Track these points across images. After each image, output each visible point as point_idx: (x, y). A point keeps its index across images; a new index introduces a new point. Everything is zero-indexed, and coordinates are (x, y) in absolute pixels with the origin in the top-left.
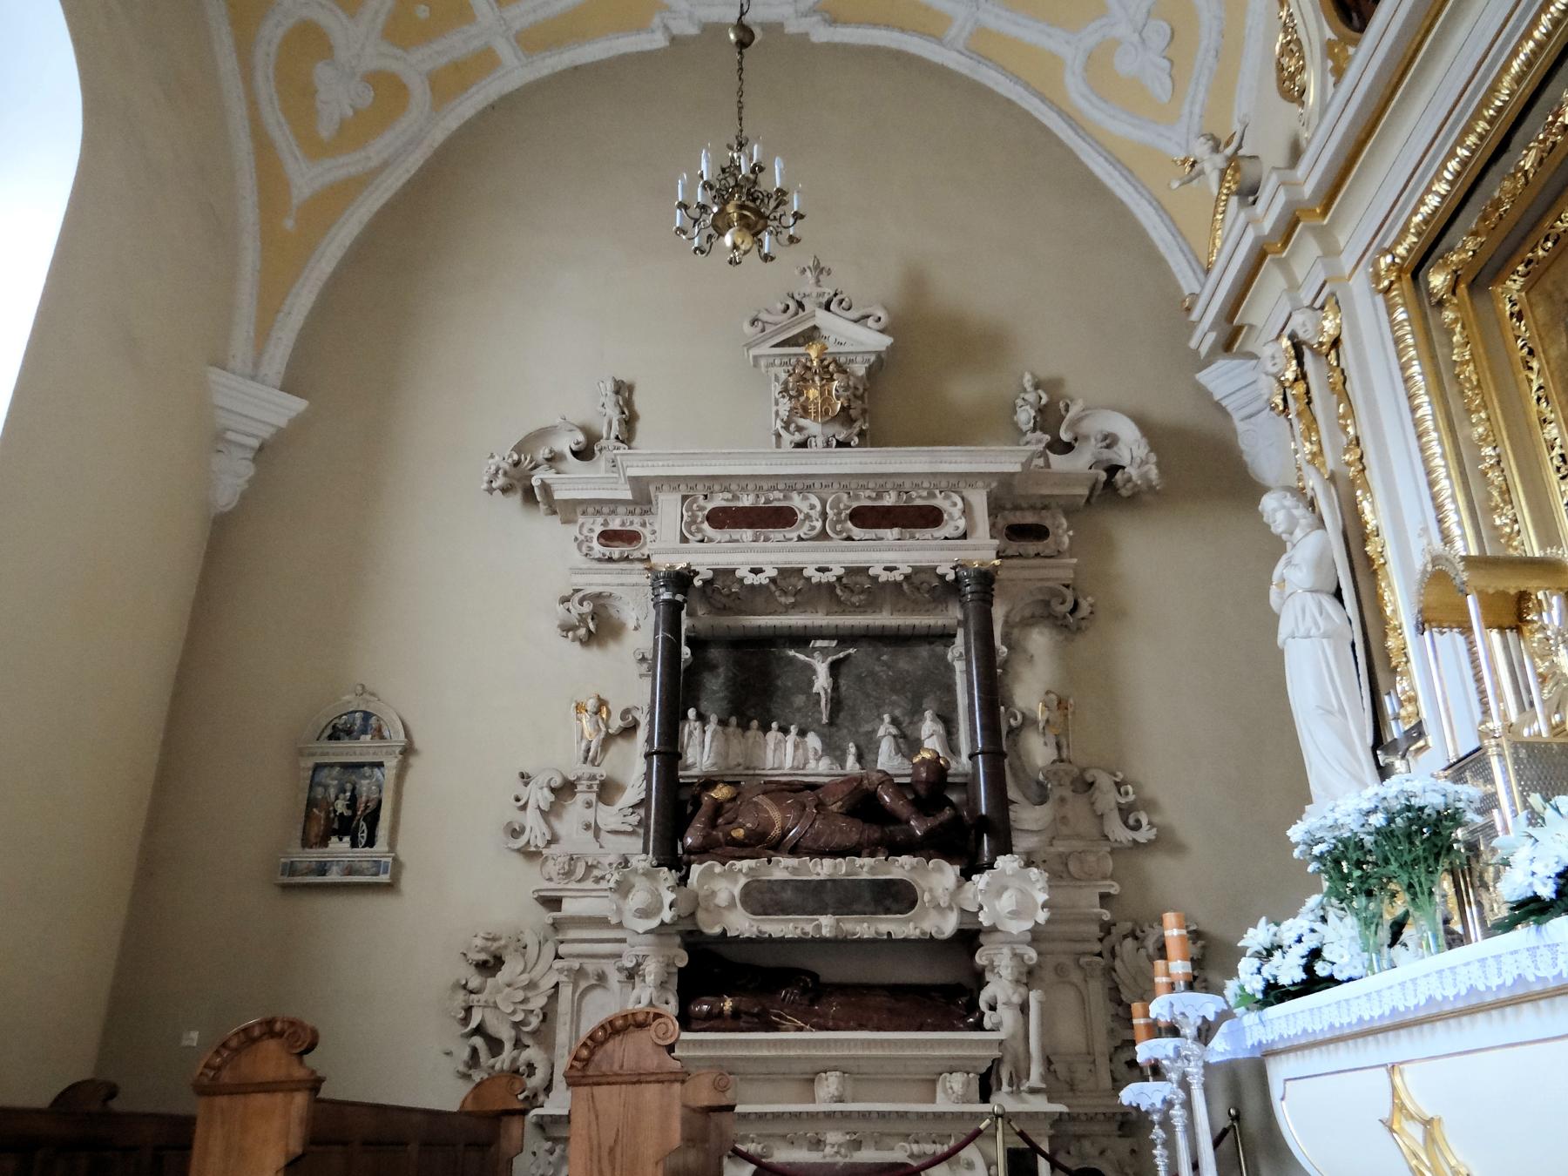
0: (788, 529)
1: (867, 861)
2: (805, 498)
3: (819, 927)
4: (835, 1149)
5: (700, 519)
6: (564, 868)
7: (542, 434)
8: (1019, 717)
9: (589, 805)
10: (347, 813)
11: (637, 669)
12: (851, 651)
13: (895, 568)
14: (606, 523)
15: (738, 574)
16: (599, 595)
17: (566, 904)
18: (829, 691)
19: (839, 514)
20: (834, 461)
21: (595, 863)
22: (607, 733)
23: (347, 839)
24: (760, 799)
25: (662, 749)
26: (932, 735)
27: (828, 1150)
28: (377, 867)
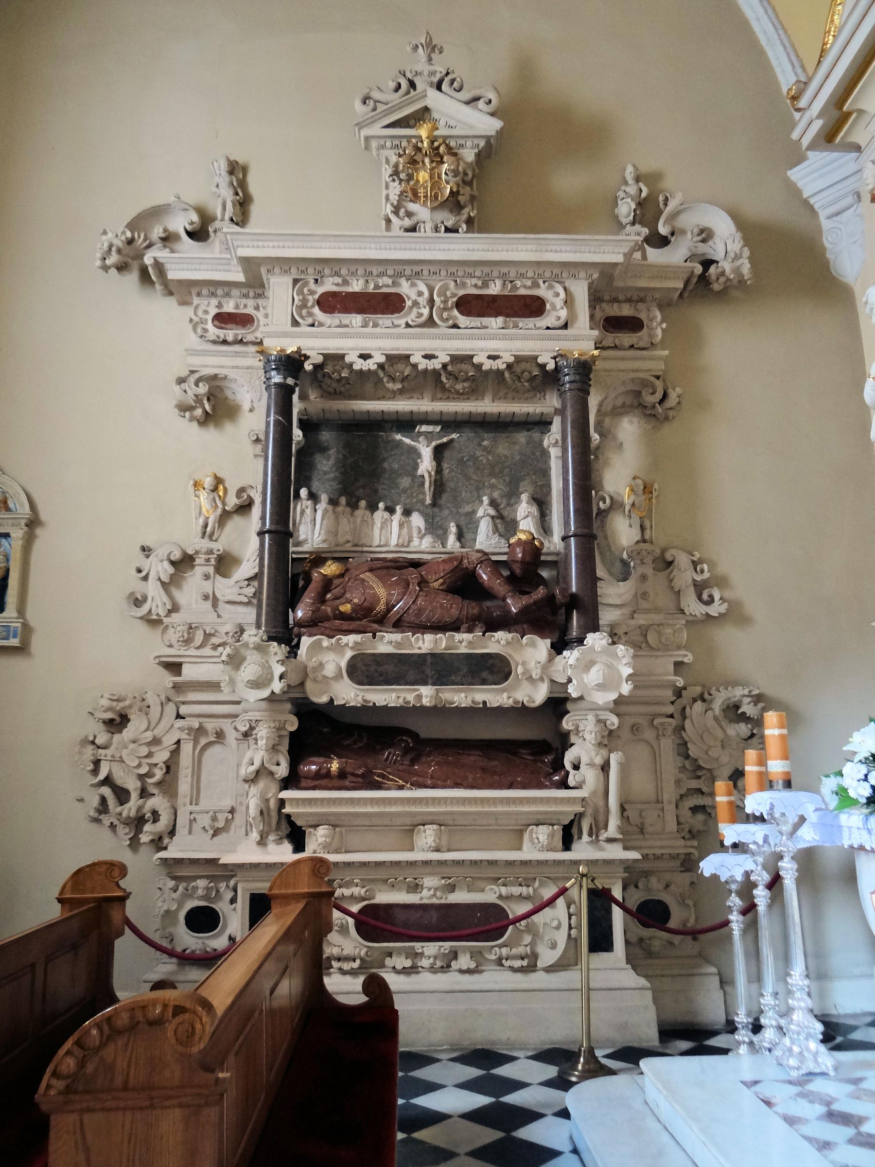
0: (396, 315)
2: (413, 285)
3: (419, 697)
4: (432, 892)
5: (310, 304)
6: (183, 636)
8: (608, 501)
9: (207, 577)
12: (454, 436)
14: (220, 306)
15: (348, 359)
16: (215, 377)
17: (185, 669)
18: (433, 473)
21: (213, 631)
22: (224, 510)
24: (367, 576)
25: (274, 528)
26: (527, 516)
27: (425, 893)
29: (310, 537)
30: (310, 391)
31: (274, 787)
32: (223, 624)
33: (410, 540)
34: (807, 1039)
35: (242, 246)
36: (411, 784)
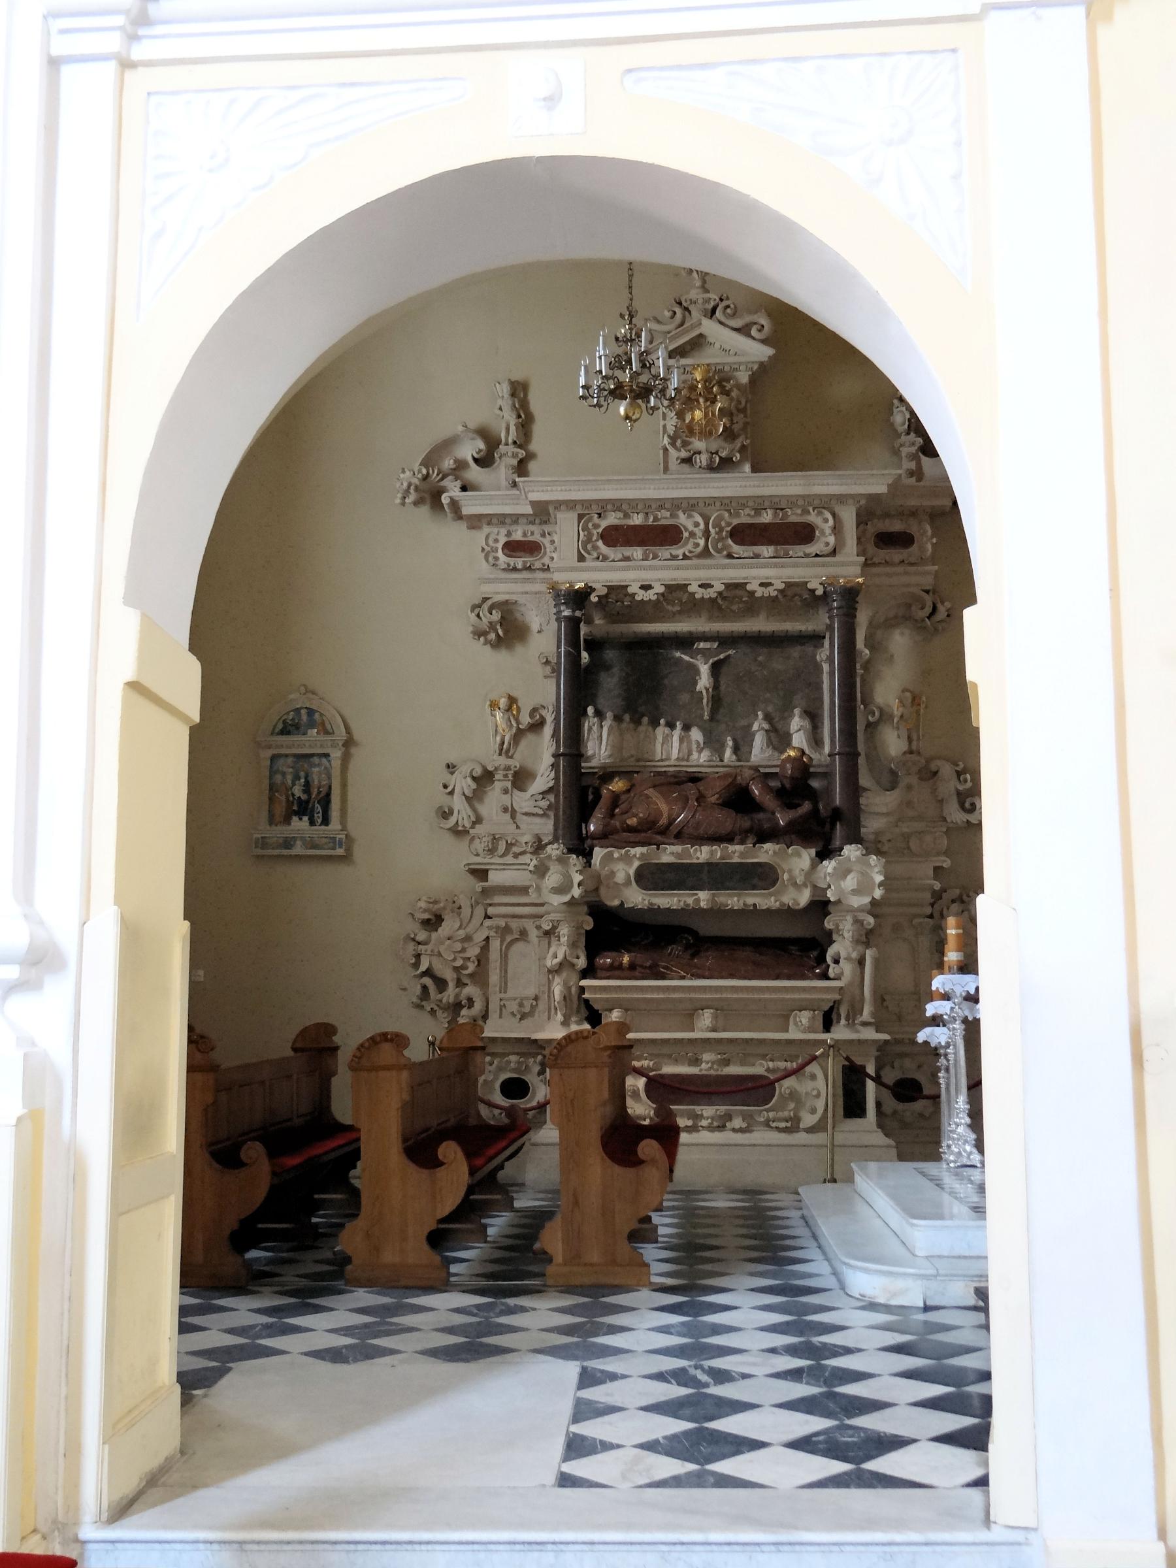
0: (675, 546)
1: (738, 848)
2: (690, 516)
3: (698, 901)
4: (710, 1065)
5: (594, 538)
6: (488, 845)
7: (447, 445)
8: (877, 714)
9: (506, 791)
10: (304, 797)
11: (540, 671)
12: (730, 652)
13: (770, 584)
14: (509, 534)
15: (630, 590)
16: (507, 602)
17: (491, 875)
18: (710, 690)
19: (721, 530)
20: (716, 485)
21: (513, 841)
22: (518, 729)
23: (306, 818)
24: (650, 792)
25: (567, 751)
26: (800, 730)
27: (704, 1066)
28: (334, 842)
29: (597, 752)
30: (594, 613)
31: (574, 977)
32: (523, 834)
33: (690, 753)
34: (964, 1144)
35: (533, 491)
36: (691, 975)
